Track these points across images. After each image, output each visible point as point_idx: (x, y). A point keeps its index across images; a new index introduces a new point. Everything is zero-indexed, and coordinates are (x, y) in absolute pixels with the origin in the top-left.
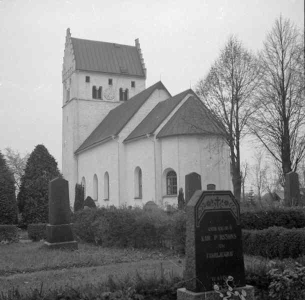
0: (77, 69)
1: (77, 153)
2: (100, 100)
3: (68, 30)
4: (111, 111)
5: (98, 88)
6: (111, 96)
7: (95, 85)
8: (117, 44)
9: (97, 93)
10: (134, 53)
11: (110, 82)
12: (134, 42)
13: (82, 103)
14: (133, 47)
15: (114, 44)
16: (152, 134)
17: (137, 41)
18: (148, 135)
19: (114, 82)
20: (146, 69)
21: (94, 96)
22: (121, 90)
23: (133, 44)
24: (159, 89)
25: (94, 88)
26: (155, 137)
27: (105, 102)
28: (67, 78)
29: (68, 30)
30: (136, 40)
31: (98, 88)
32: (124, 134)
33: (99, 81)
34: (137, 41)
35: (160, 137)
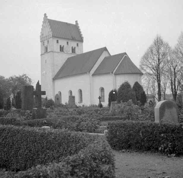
0: (53, 36)
1: (54, 79)
2: (63, 52)
3: (45, 14)
4: (68, 58)
5: (62, 46)
6: (68, 50)
7: (73, 46)
8: (68, 23)
9: (62, 49)
10: (76, 27)
11: (67, 43)
12: (75, 22)
13: (55, 53)
14: (74, 25)
15: (67, 23)
16: (112, 73)
17: (76, 22)
18: (111, 73)
19: (69, 43)
20: (83, 37)
21: (61, 50)
22: (72, 47)
23: (74, 23)
24: (105, 50)
25: (60, 46)
26: (113, 74)
27: (65, 53)
28: (43, 40)
29: (45, 14)
30: (76, 21)
31: (62, 46)
32: (92, 72)
33: (63, 43)
34: (76, 22)
35: (116, 74)
